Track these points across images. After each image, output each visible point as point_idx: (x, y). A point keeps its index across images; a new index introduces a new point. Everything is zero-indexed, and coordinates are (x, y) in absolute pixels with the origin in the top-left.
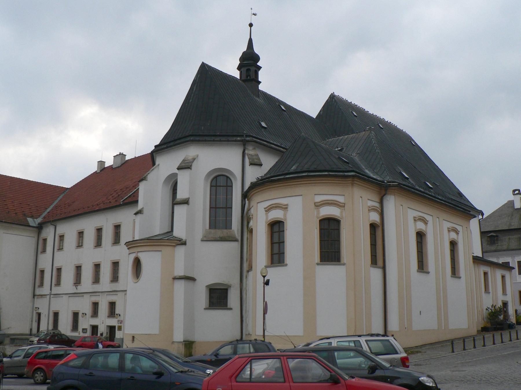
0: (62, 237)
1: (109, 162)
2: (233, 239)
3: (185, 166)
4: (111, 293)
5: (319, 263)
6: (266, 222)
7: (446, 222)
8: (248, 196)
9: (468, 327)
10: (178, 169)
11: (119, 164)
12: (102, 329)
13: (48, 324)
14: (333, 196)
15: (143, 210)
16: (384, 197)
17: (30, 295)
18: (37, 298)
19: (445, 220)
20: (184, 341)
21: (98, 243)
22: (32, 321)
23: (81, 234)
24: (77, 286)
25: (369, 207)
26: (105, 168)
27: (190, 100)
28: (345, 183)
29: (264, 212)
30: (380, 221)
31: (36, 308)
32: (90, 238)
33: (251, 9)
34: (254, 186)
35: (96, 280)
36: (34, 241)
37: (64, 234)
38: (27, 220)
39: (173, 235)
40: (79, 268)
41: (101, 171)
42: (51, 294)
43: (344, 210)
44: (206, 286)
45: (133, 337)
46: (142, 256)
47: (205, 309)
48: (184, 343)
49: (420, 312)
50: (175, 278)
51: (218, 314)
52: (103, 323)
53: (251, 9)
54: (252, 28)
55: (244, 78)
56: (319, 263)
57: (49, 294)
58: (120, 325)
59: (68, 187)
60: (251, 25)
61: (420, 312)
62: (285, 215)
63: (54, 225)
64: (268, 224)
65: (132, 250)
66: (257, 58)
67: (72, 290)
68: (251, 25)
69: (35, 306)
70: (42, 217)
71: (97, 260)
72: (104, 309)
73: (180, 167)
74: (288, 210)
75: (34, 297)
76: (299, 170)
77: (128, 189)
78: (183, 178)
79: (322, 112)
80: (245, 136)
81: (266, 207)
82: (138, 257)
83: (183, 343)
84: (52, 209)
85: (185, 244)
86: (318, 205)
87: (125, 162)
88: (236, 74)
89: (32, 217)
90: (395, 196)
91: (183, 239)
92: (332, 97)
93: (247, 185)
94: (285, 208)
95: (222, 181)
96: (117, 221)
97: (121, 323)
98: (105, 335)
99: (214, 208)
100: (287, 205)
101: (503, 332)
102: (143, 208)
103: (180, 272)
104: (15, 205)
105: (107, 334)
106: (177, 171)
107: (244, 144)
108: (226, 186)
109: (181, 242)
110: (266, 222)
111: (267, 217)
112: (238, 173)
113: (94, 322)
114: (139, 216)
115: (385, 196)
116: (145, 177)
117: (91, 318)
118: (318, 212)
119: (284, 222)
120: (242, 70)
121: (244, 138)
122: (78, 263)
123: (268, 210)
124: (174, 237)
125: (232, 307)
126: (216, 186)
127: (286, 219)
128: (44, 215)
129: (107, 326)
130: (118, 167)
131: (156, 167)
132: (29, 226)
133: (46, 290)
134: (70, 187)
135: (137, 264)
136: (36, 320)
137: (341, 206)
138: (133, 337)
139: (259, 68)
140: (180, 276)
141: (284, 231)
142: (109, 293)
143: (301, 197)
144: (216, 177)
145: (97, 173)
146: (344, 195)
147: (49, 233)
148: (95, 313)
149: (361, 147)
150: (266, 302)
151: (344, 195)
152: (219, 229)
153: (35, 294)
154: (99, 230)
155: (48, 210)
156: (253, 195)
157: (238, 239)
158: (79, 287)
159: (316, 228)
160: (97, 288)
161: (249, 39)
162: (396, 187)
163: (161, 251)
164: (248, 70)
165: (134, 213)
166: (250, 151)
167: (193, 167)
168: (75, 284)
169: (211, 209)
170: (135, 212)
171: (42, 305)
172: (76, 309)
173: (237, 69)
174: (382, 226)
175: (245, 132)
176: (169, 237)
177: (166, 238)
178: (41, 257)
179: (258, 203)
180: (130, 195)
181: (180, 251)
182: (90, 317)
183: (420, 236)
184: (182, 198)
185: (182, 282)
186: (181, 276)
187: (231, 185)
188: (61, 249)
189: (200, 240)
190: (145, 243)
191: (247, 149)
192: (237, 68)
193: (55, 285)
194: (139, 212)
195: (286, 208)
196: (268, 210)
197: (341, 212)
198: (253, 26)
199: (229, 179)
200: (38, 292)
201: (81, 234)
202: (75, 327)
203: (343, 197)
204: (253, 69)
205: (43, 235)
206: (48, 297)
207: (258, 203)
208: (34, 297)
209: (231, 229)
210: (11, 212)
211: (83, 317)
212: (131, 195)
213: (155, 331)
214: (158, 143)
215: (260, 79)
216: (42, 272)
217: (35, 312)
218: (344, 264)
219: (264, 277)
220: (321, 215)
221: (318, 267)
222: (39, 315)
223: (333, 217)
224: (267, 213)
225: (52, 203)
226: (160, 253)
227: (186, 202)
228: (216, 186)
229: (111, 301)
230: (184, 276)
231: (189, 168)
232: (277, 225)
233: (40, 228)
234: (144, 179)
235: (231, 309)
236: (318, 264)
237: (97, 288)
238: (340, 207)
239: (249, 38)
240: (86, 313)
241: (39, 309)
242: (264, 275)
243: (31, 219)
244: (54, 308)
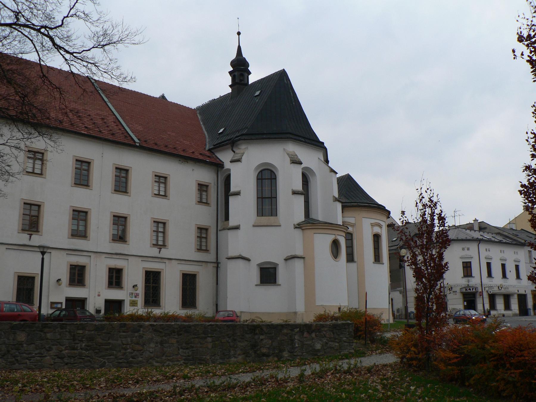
4: (22, 248)
33: (238, 18)
37: (167, 221)
44: (257, 265)
53: (238, 18)
54: (240, 36)
58: (134, 299)
60: (239, 33)
68: (239, 33)
92: (251, 73)
95: (267, 175)
101: (210, 313)
126: (262, 179)
144: (261, 171)
161: (238, 46)
169: (258, 199)
187: (275, 178)
192: (251, 74)
198: (241, 35)
228: (262, 179)
235: (280, 285)
239: (238, 45)
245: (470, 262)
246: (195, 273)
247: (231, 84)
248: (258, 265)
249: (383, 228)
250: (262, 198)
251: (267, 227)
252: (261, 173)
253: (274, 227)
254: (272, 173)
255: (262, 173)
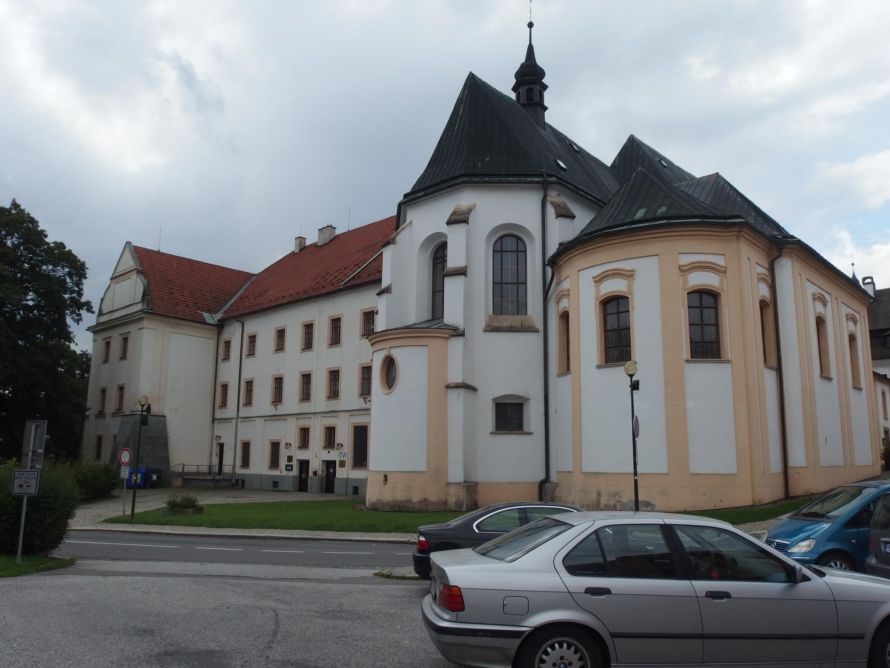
0: (253, 339)
1: (312, 238)
2: (532, 330)
3: (459, 219)
5: (690, 359)
6: (596, 299)
7: (845, 306)
8: (558, 264)
9: (872, 464)
10: (449, 223)
11: (327, 237)
12: (316, 465)
13: (235, 458)
14: (711, 256)
15: (391, 289)
16: (775, 261)
17: (209, 418)
18: (218, 423)
19: (844, 303)
20: (465, 482)
21: (308, 344)
22: (211, 455)
23: (281, 334)
24: (277, 405)
25: (759, 275)
26: (305, 247)
27: (454, 127)
28: (723, 236)
29: (594, 284)
30: (771, 298)
31: (217, 436)
32: (294, 338)
34: (567, 249)
35: (306, 396)
36: (213, 343)
38: (203, 315)
39: (443, 322)
40: (279, 382)
41: (300, 251)
42: (238, 418)
43: (725, 277)
45: (386, 476)
46: (396, 354)
47: (491, 433)
48: (465, 484)
49: (826, 438)
50: (448, 387)
51: (510, 440)
52: (316, 457)
55: (523, 100)
56: (690, 359)
57: (235, 417)
58: (342, 459)
59: (255, 273)
60: (531, 25)
61: (826, 438)
62: (630, 287)
63: (241, 322)
64: (600, 302)
65: (377, 347)
66: (541, 73)
67: (270, 410)
68: (531, 25)
69: (216, 434)
70: (223, 312)
71: (306, 369)
72: (317, 437)
73: (455, 217)
74: (634, 279)
75: (213, 422)
76: (649, 216)
77: (347, 270)
78: (456, 239)
79: (617, 162)
80: (545, 175)
81: (595, 275)
82: (391, 355)
83: (464, 484)
84: (236, 302)
85: (462, 334)
86: (685, 270)
87: (335, 237)
88: (513, 96)
89: (209, 311)
90: (792, 259)
91: (460, 327)
93: (552, 249)
94: (629, 275)
95: (510, 244)
96: (335, 314)
97: (344, 456)
98: (320, 473)
99: (499, 285)
100: (633, 271)
102: (391, 285)
103: (456, 377)
104: (185, 295)
105: (323, 473)
106: (444, 229)
107: (545, 187)
108: (516, 252)
109: (457, 333)
110: (595, 299)
111: (598, 291)
112: (536, 232)
113: (303, 455)
114: (385, 296)
115: (779, 259)
116: (393, 239)
117: (299, 449)
118: (686, 281)
119: (628, 298)
120: (520, 90)
121: (544, 178)
122: (278, 373)
123: (599, 280)
124: (444, 324)
125: (531, 431)
126: (502, 251)
127: (631, 293)
128: (224, 309)
129: (323, 461)
130: (326, 244)
131: (407, 226)
132: (206, 323)
133: (230, 411)
134: (258, 273)
135: (390, 364)
136: (217, 454)
137: (720, 272)
138: (386, 476)
139: (545, 87)
140: (456, 384)
141: (629, 311)
142: (325, 414)
143: (655, 259)
144: (501, 238)
145: (295, 254)
146: (724, 255)
147: (234, 333)
148: (304, 443)
149: (708, 197)
150: (636, 417)
151: (724, 255)
152: (508, 314)
153: (215, 417)
154: (309, 328)
155: (230, 303)
156: (562, 265)
157: (538, 329)
158: (279, 407)
159: (683, 306)
160: (307, 407)
162: (796, 245)
163: (427, 346)
164: (530, 91)
165: (376, 293)
166: (554, 196)
167: (470, 221)
168: (273, 402)
170: (377, 291)
171: (226, 434)
172: (275, 437)
173: (512, 89)
174: (773, 304)
175: (543, 170)
176: (438, 325)
177: (435, 327)
178: (223, 366)
179: (579, 271)
180: (354, 276)
181: (456, 345)
182: (297, 448)
183: (820, 322)
184: (454, 268)
185: (461, 391)
186: (459, 383)
188: (251, 353)
189: (482, 330)
190: (400, 333)
191: (549, 195)
193: (244, 404)
194: (387, 290)
195: (632, 276)
196: (599, 280)
197: (721, 281)
199: (521, 242)
200: (219, 414)
201: (281, 334)
202: (274, 463)
203: (722, 258)
204: (537, 88)
205: (225, 336)
206: (234, 421)
207: (579, 271)
208: (213, 422)
209: (527, 314)
210: (179, 304)
211: (287, 449)
212: (355, 275)
213: (421, 465)
214: (408, 190)
215: (546, 104)
216: (225, 387)
217: (215, 443)
218: (728, 362)
219: (631, 376)
220: (689, 286)
221: (687, 365)
222: (221, 446)
223: (714, 289)
224: (597, 284)
225: (234, 293)
226: (425, 348)
227: (461, 272)
228: (502, 251)
229: (328, 426)
230: (463, 383)
231: (465, 221)
232: (614, 303)
233: (220, 326)
234: (391, 241)
235: (531, 433)
236: (687, 361)
237: (307, 407)
238: (719, 272)
240: (291, 443)
241: (220, 437)
242: (631, 373)
243: (208, 314)
244: (243, 436)
245: (345, 467)
246: (366, 424)
247: (550, 118)
248: (493, 400)
249: (827, 306)
250: (518, 283)
251: (398, 339)
252: (500, 240)
253: (849, 308)
254: (519, 241)
255: (502, 240)
